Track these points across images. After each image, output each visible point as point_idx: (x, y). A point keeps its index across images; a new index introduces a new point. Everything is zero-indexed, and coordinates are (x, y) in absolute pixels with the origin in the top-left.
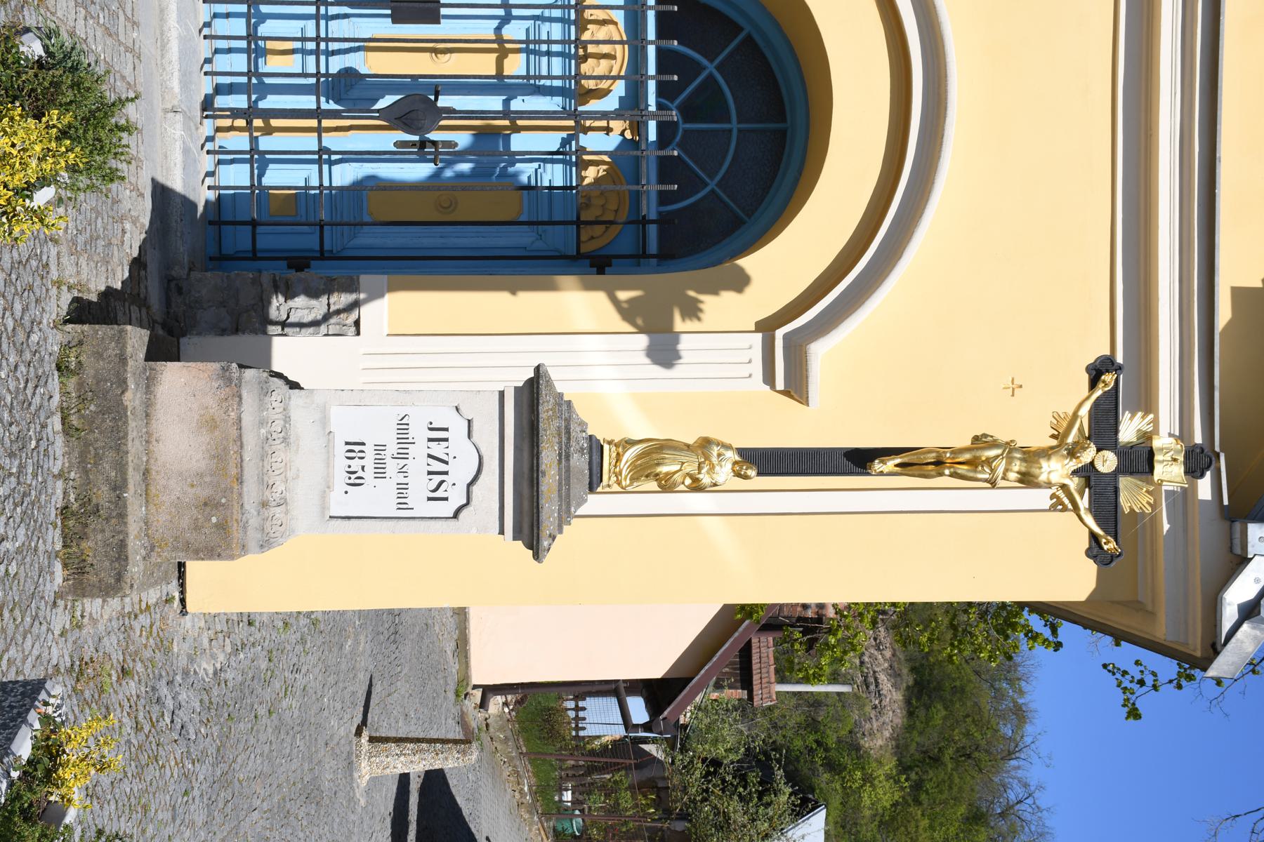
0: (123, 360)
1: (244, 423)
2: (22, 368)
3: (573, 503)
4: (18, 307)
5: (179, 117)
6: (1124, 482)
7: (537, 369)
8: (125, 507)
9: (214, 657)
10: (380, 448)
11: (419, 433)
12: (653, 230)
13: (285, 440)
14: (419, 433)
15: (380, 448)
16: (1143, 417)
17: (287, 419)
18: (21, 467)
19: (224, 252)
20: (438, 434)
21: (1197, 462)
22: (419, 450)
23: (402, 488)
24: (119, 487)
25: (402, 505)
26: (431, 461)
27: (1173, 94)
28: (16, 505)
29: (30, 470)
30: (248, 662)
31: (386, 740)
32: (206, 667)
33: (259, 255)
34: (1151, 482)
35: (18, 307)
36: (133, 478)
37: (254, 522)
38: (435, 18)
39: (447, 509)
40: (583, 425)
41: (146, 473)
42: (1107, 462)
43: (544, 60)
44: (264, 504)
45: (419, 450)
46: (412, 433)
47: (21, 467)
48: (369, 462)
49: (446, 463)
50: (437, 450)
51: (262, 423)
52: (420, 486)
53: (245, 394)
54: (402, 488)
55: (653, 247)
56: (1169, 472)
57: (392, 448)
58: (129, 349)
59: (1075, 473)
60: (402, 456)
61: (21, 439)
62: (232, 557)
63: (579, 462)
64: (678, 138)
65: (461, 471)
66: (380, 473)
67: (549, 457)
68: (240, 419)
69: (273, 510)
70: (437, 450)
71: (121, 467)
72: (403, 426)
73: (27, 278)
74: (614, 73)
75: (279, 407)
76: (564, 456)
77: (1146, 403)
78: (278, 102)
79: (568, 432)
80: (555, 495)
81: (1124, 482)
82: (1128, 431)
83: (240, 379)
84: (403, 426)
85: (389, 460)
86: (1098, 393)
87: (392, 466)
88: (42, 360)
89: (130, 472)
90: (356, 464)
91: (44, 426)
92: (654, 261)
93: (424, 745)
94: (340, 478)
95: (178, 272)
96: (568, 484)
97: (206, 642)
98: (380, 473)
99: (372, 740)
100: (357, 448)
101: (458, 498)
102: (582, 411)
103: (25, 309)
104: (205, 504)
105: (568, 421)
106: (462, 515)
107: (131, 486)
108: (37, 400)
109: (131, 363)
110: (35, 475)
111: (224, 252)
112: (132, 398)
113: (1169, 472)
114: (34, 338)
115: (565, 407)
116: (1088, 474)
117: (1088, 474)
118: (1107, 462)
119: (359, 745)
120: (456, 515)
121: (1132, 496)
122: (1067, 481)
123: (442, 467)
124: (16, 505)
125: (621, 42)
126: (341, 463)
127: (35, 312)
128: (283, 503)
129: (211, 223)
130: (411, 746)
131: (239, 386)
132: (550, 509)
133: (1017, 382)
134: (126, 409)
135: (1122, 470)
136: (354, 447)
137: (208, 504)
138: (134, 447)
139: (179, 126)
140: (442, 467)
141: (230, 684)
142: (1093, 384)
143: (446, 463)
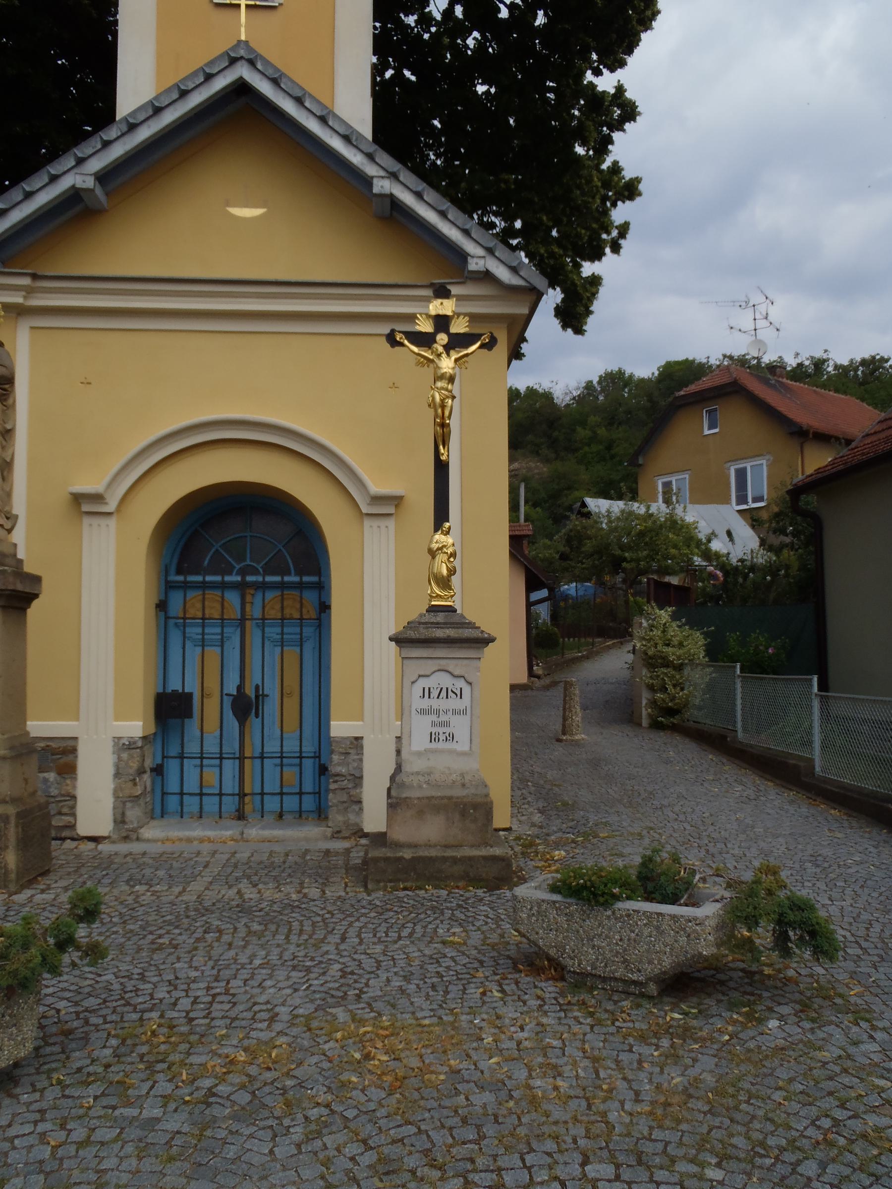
0: (386, 859)
1: (421, 796)
2: (396, 909)
3: (463, 621)
4: (363, 911)
5: (246, 831)
6: (454, 329)
7: (391, 639)
8: (465, 857)
9: (532, 813)
10: (434, 724)
11: (425, 703)
12: (306, 579)
13: (429, 774)
14: (425, 703)
15: (434, 724)
16: (418, 319)
17: (418, 773)
18: (447, 908)
19: (314, 809)
20: (427, 693)
21: (442, 293)
22: (435, 703)
23: (455, 712)
24: (455, 860)
25: (464, 712)
26: (441, 697)
27: (241, 303)
28: (469, 911)
29: (448, 905)
30: (533, 796)
31: (564, 726)
32: (537, 818)
33: (317, 790)
34: (452, 317)
35: (363, 911)
36: (449, 853)
37: (473, 791)
38: (190, 695)
39: (467, 690)
40: (421, 615)
41: (447, 846)
42: (442, 338)
43: (285, 636)
44: (463, 785)
45: (435, 703)
46: (425, 707)
47: (447, 908)
48: (441, 730)
49: (441, 689)
50: (435, 693)
51: (420, 787)
52: (454, 703)
53: (404, 795)
54: (455, 712)
55: (314, 579)
56: (446, 307)
57: (434, 718)
58: (381, 855)
59: (448, 355)
60: (438, 712)
61: (433, 908)
62: (492, 802)
63: (440, 617)
64: (254, 564)
65: (445, 681)
66: (446, 724)
67: (440, 633)
68: (419, 798)
69: (467, 781)
70: (435, 693)
71: (444, 859)
72: (422, 712)
73: (347, 906)
74: (220, 599)
75: (412, 777)
76: (437, 625)
77: (412, 318)
78: (253, 777)
79: (426, 623)
80: (460, 631)
81: (454, 329)
82: (425, 327)
83: (397, 798)
84: (422, 712)
85: (440, 720)
86: (406, 342)
87: (443, 718)
88: (389, 900)
89: (446, 854)
90: (442, 737)
91: (424, 898)
92: (322, 579)
93: (567, 706)
94: (449, 746)
95: (329, 832)
96: (453, 623)
97: (524, 818)
98: (446, 724)
99: (564, 733)
100: (433, 737)
101: (461, 683)
102: (413, 616)
103: (364, 907)
104: (463, 816)
105: (420, 623)
106: (470, 681)
107: (454, 854)
108: (411, 902)
109: (389, 855)
110: (451, 902)
111: (314, 809)
112: (407, 854)
113: (446, 307)
114: (378, 903)
115: (410, 625)
116: (448, 348)
117: (448, 348)
118: (442, 338)
119: (566, 740)
120: (471, 684)
121: (459, 327)
122: (453, 358)
123: (444, 691)
124: (469, 911)
125: (204, 594)
126: (441, 745)
127: (364, 903)
128: (462, 775)
129: (300, 816)
130: (567, 713)
131: (400, 798)
132: (467, 633)
133: (391, 385)
134: (413, 857)
135: (446, 331)
136: (433, 738)
137: (463, 814)
138: (433, 853)
139: (250, 831)
140: (444, 691)
141: (546, 805)
142: (402, 344)
143: (441, 689)
